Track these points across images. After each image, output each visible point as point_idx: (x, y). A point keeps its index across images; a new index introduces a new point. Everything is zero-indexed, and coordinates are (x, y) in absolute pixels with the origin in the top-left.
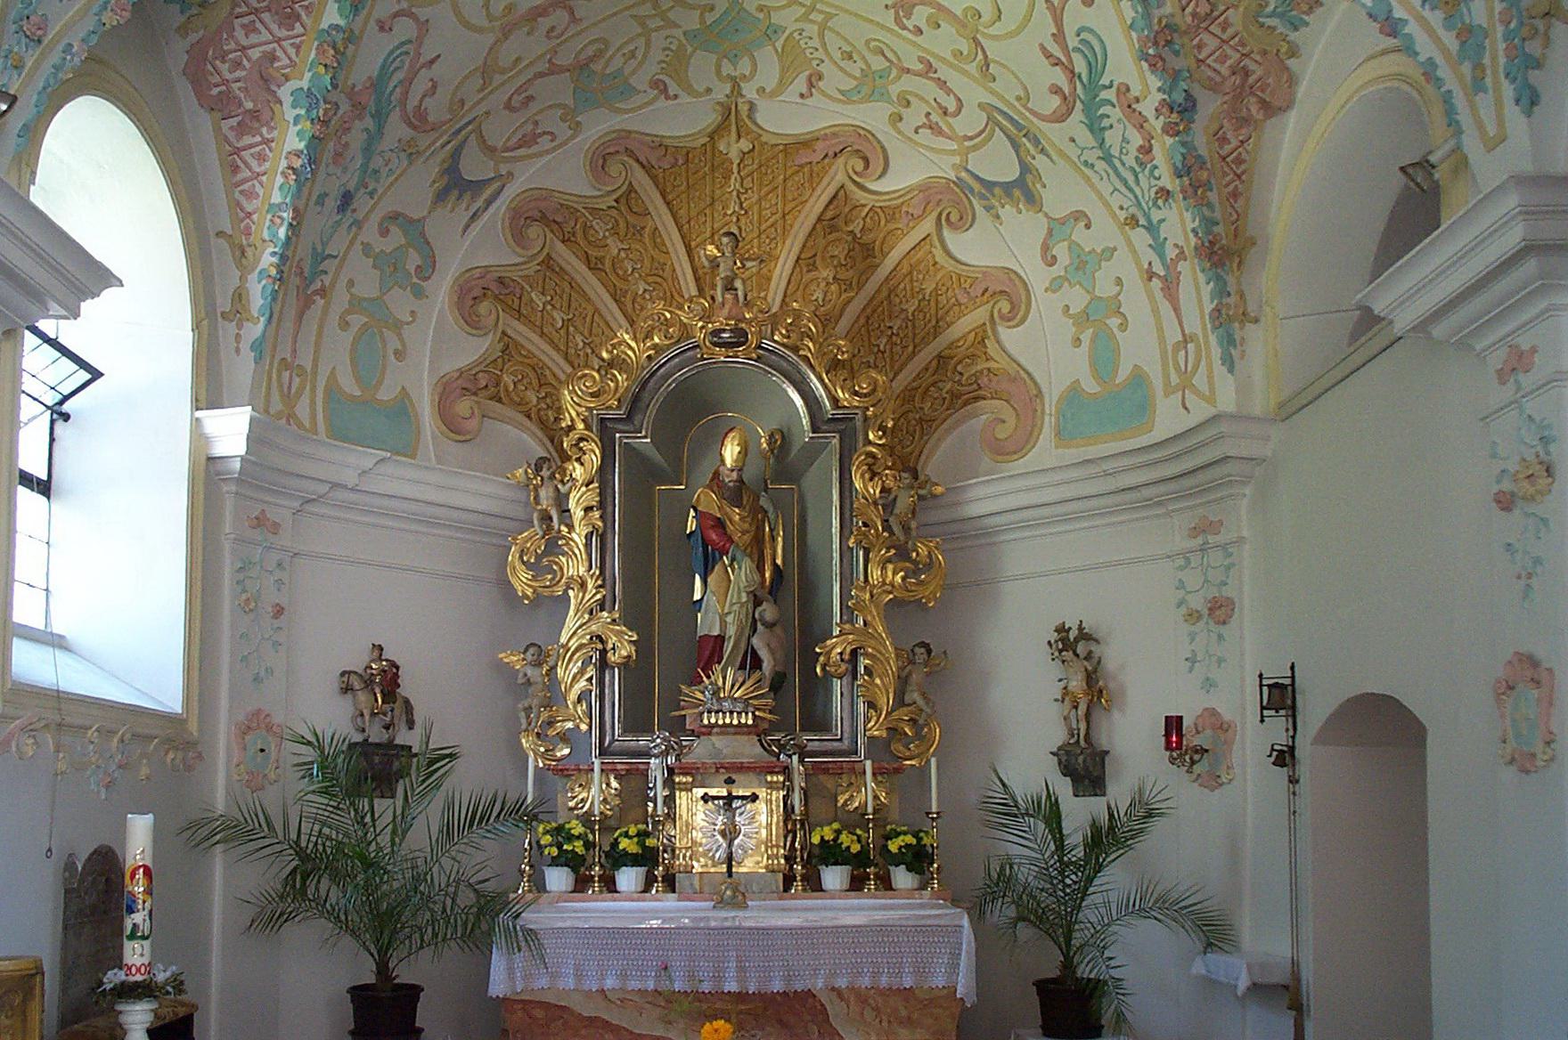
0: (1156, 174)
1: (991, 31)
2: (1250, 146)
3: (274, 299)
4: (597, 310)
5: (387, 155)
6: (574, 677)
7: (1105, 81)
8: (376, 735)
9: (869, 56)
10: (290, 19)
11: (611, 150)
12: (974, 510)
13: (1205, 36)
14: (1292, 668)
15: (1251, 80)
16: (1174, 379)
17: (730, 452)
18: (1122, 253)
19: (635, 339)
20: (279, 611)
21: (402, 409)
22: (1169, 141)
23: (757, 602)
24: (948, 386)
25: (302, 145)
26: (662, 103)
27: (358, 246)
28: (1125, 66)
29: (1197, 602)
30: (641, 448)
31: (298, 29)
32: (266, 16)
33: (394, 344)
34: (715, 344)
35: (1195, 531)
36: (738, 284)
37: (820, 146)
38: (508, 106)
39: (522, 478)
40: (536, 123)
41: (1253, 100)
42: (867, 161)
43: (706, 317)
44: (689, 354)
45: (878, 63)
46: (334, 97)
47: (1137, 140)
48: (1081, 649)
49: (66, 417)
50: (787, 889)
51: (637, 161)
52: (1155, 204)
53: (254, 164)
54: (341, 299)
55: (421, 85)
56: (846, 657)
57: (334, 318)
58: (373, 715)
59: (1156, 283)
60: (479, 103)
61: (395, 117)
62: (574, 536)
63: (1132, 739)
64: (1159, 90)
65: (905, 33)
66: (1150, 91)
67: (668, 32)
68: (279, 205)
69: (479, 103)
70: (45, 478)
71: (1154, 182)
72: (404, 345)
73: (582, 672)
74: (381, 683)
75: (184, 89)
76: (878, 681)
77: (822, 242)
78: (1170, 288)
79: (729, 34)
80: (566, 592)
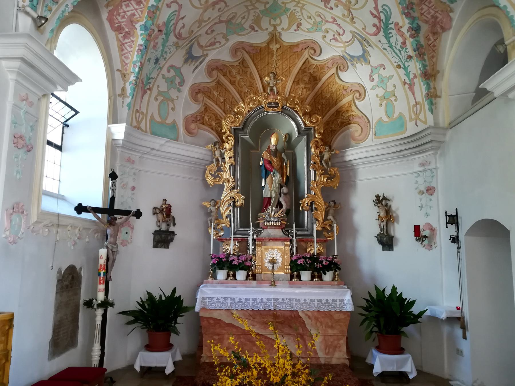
0: (407, 51)
1: (354, 7)
2: (437, 41)
3: (134, 90)
4: (233, 97)
5: (170, 47)
6: (225, 210)
7: (391, 22)
8: (164, 227)
10: (139, 3)
11: (238, 47)
13: (424, 6)
14: (457, 210)
15: (438, 20)
16: (413, 116)
17: (273, 140)
18: (396, 76)
19: (245, 105)
20: (133, 188)
21: (174, 126)
22: (411, 40)
23: (281, 187)
25: (143, 43)
26: (253, 32)
27: (160, 76)
29: (423, 188)
30: (246, 139)
31: (142, 6)
33: (171, 106)
34: (269, 107)
35: (422, 165)
36: (275, 88)
37: (301, 47)
38: (207, 33)
39: (210, 148)
40: (215, 39)
41: (439, 26)
43: (266, 98)
44: (261, 110)
45: (319, 19)
46: (153, 27)
47: (401, 40)
48: (384, 202)
49: (68, 126)
53: (128, 48)
54: (155, 92)
55: (180, 24)
56: (309, 204)
58: (163, 221)
60: (198, 31)
61: (172, 34)
63: (402, 232)
64: (408, 24)
66: (405, 24)
69: (198, 31)
70: (60, 145)
71: (406, 54)
72: (174, 105)
75: (107, 25)
76: (319, 212)
77: (301, 76)
78: (411, 87)
79: (274, 11)
80: (223, 183)
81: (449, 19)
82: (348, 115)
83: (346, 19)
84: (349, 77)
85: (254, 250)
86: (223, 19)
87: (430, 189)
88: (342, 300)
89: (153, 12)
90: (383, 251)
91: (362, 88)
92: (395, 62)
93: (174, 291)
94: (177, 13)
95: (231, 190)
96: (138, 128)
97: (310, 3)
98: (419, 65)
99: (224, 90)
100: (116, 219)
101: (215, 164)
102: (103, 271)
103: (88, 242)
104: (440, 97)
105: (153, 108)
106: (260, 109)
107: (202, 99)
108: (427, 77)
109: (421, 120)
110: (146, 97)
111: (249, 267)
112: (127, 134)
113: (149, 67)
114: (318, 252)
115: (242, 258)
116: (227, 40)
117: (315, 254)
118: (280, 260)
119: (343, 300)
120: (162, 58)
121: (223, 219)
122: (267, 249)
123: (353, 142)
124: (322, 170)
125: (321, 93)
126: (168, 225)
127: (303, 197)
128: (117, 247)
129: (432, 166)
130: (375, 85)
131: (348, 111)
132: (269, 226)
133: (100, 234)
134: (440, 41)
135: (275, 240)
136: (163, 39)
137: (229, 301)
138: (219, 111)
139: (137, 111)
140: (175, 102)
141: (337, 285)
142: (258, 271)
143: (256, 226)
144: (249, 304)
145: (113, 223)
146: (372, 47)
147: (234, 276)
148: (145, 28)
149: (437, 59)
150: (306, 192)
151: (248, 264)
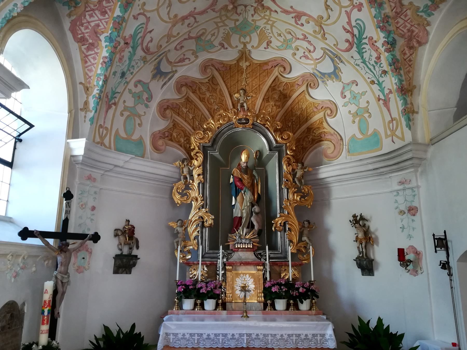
0: (382, 66)
1: (326, 23)
3: (98, 104)
4: (202, 114)
5: (137, 61)
6: (192, 230)
7: (364, 36)
8: (126, 251)
9: (286, 35)
12: (322, 176)
13: (399, 20)
14: (445, 232)
15: (414, 34)
16: (389, 133)
17: (244, 157)
18: (369, 93)
19: (214, 121)
20: (93, 208)
21: (140, 142)
22: (387, 54)
23: (253, 206)
24: (311, 137)
25: (107, 55)
26: (223, 50)
28: (372, 31)
29: (403, 208)
30: (215, 155)
32: (97, 12)
33: (138, 121)
34: (239, 123)
35: (401, 183)
36: (245, 105)
38: (176, 49)
39: (178, 165)
40: (184, 55)
41: (415, 40)
42: (285, 68)
43: (236, 114)
44: (231, 126)
45: (289, 37)
46: (118, 39)
47: (375, 55)
48: (361, 223)
49: (21, 141)
50: (265, 309)
51: (215, 68)
52: (381, 76)
53: (92, 60)
54: (121, 107)
55: (148, 38)
56: (282, 224)
57: (118, 113)
58: (125, 244)
59: (381, 102)
61: (139, 48)
62: (194, 184)
63: (384, 254)
65: (298, 26)
66: (380, 38)
67: (224, 28)
68: (100, 74)
69: (166, 47)
70: (10, 161)
71: (380, 69)
73: (196, 228)
74: (128, 233)
75: (69, 36)
76: (293, 233)
77: (270, 94)
78: (386, 103)
81: (426, 33)
82: (319, 132)
83: (317, 36)
84: (319, 94)
85: (224, 275)
86: (191, 35)
87: (413, 209)
88: (323, 335)
89: (119, 23)
90: (363, 275)
91: (334, 106)
92: (369, 78)
93: (133, 326)
94: (144, 26)
95: (199, 209)
96: (102, 144)
97: (280, 20)
98: (394, 80)
99: (194, 107)
100: (68, 245)
101: (183, 181)
102: (48, 308)
103: (34, 272)
104: (417, 113)
105: (119, 124)
106: (231, 126)
107: (170, 115)
108: (403, 92)
109: (397, 137)
110: (111, 112)
111: (218, 295)
112: (87, 149)
113: (114, 81)
114: (293, 277)
115: (210, 285)
116: (197, 57)
117: (291, 280)
118: (252, 286)
119: (324, 335)
120: (128, 72)
121: (191, 241)
122: (238, 275)
123: (325, 160)
124: (295, 188)
125: (291, 110)
126: (131, 248)
127: (275, 217)
128: (69, 276)
129: (413, 184)
130: (348, 102)
131: (319, 128)
132: (240, 248)
133: (50, 261)
134: (416, 55)
135: (247, 264)
136: (130, 52)
137: (196, 337)
138: (188, 128)
139: (101, 126)
140: (142, 117)
141: (315, 315)
142: (228, 299)
143: (226, 248)
144: (219, 341)
145: (64, 250)
146: (344, 63)
147: (202, 305)
148: (110, 39)
149: (413, 74)
150: (278, 211)
151: (217, 292)
